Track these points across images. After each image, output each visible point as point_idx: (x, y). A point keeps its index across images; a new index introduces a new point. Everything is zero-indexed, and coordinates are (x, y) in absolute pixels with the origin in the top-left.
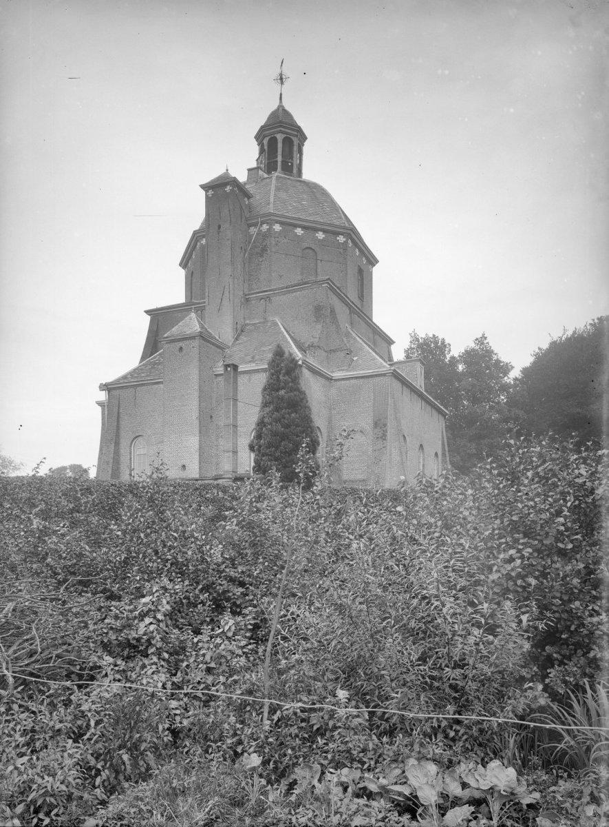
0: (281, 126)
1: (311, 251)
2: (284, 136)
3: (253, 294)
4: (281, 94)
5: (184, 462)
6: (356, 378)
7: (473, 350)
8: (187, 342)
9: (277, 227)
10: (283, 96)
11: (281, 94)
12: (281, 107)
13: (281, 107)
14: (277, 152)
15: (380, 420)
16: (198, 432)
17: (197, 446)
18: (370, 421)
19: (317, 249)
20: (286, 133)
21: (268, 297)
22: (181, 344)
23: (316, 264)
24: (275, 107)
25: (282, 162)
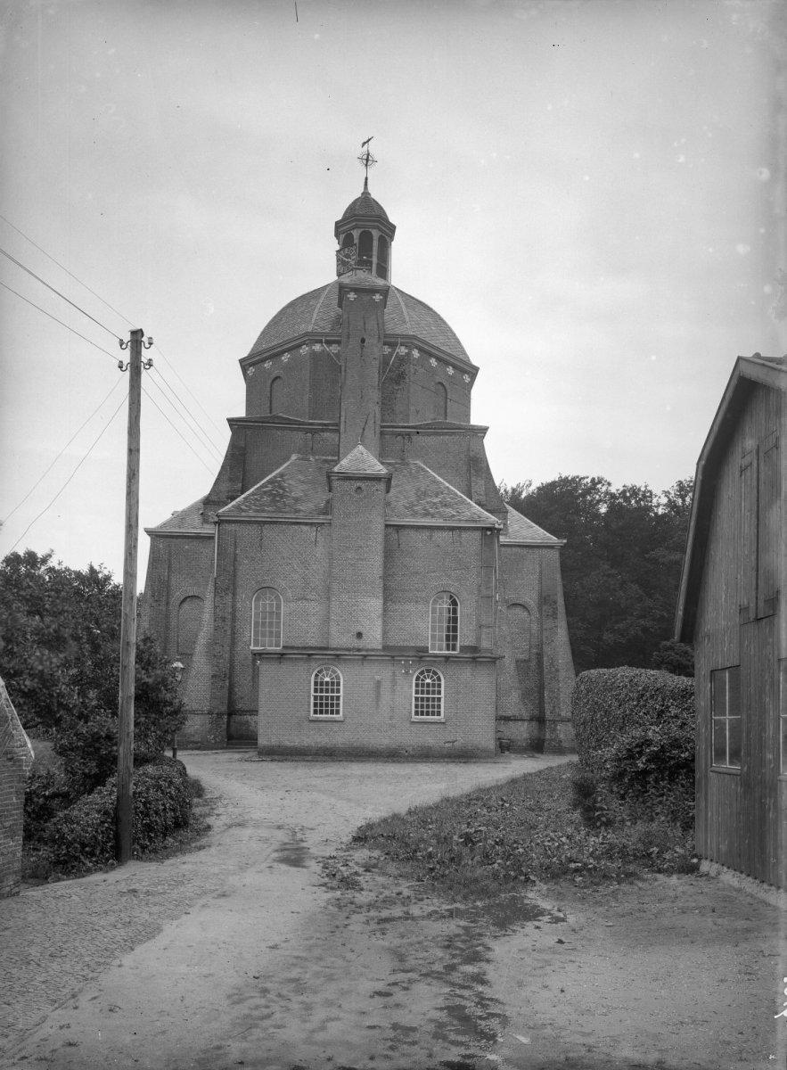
0: (378, 221)
1: (441, 388)
2: (360, 231)
3: (389, 427)
4: (366, 179)
5: (355, 631)
6: (519, 546)
7: (20, 556)
8: (369, 483)
9: (416, 354)
10: (369, 183)
11: (366, 179)
12: (366, 194)
13: (366, 194)
14: (372, 250)
15: (549, 596)
16: (381, 590)
17: (380, 611)
18: (535, 596)
19: (447, 386)
20: (364, 227)
21: (408, 434)
22: (359, 484)
23: (446, 403)
24: (357, 193)
25: (378, 264)
